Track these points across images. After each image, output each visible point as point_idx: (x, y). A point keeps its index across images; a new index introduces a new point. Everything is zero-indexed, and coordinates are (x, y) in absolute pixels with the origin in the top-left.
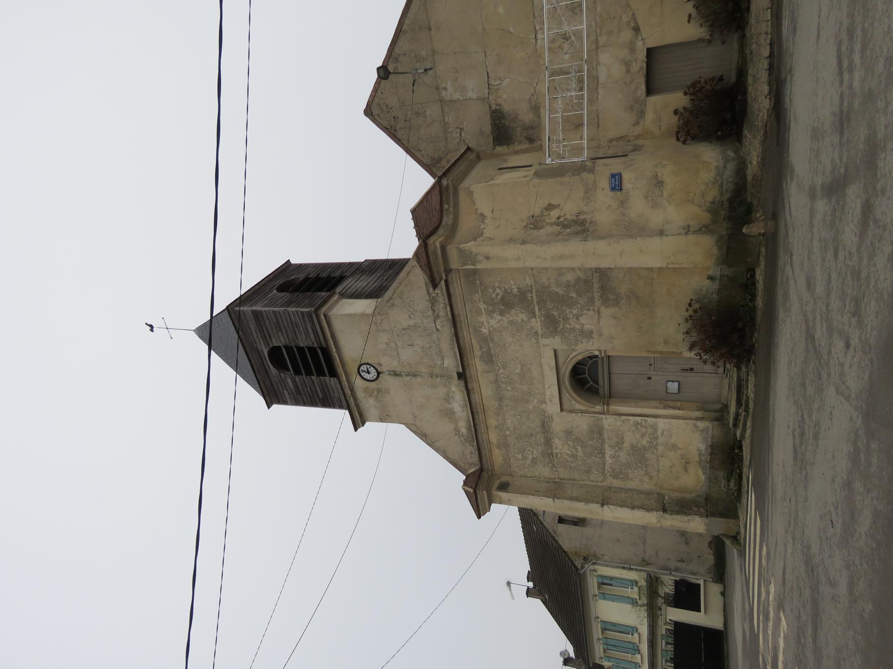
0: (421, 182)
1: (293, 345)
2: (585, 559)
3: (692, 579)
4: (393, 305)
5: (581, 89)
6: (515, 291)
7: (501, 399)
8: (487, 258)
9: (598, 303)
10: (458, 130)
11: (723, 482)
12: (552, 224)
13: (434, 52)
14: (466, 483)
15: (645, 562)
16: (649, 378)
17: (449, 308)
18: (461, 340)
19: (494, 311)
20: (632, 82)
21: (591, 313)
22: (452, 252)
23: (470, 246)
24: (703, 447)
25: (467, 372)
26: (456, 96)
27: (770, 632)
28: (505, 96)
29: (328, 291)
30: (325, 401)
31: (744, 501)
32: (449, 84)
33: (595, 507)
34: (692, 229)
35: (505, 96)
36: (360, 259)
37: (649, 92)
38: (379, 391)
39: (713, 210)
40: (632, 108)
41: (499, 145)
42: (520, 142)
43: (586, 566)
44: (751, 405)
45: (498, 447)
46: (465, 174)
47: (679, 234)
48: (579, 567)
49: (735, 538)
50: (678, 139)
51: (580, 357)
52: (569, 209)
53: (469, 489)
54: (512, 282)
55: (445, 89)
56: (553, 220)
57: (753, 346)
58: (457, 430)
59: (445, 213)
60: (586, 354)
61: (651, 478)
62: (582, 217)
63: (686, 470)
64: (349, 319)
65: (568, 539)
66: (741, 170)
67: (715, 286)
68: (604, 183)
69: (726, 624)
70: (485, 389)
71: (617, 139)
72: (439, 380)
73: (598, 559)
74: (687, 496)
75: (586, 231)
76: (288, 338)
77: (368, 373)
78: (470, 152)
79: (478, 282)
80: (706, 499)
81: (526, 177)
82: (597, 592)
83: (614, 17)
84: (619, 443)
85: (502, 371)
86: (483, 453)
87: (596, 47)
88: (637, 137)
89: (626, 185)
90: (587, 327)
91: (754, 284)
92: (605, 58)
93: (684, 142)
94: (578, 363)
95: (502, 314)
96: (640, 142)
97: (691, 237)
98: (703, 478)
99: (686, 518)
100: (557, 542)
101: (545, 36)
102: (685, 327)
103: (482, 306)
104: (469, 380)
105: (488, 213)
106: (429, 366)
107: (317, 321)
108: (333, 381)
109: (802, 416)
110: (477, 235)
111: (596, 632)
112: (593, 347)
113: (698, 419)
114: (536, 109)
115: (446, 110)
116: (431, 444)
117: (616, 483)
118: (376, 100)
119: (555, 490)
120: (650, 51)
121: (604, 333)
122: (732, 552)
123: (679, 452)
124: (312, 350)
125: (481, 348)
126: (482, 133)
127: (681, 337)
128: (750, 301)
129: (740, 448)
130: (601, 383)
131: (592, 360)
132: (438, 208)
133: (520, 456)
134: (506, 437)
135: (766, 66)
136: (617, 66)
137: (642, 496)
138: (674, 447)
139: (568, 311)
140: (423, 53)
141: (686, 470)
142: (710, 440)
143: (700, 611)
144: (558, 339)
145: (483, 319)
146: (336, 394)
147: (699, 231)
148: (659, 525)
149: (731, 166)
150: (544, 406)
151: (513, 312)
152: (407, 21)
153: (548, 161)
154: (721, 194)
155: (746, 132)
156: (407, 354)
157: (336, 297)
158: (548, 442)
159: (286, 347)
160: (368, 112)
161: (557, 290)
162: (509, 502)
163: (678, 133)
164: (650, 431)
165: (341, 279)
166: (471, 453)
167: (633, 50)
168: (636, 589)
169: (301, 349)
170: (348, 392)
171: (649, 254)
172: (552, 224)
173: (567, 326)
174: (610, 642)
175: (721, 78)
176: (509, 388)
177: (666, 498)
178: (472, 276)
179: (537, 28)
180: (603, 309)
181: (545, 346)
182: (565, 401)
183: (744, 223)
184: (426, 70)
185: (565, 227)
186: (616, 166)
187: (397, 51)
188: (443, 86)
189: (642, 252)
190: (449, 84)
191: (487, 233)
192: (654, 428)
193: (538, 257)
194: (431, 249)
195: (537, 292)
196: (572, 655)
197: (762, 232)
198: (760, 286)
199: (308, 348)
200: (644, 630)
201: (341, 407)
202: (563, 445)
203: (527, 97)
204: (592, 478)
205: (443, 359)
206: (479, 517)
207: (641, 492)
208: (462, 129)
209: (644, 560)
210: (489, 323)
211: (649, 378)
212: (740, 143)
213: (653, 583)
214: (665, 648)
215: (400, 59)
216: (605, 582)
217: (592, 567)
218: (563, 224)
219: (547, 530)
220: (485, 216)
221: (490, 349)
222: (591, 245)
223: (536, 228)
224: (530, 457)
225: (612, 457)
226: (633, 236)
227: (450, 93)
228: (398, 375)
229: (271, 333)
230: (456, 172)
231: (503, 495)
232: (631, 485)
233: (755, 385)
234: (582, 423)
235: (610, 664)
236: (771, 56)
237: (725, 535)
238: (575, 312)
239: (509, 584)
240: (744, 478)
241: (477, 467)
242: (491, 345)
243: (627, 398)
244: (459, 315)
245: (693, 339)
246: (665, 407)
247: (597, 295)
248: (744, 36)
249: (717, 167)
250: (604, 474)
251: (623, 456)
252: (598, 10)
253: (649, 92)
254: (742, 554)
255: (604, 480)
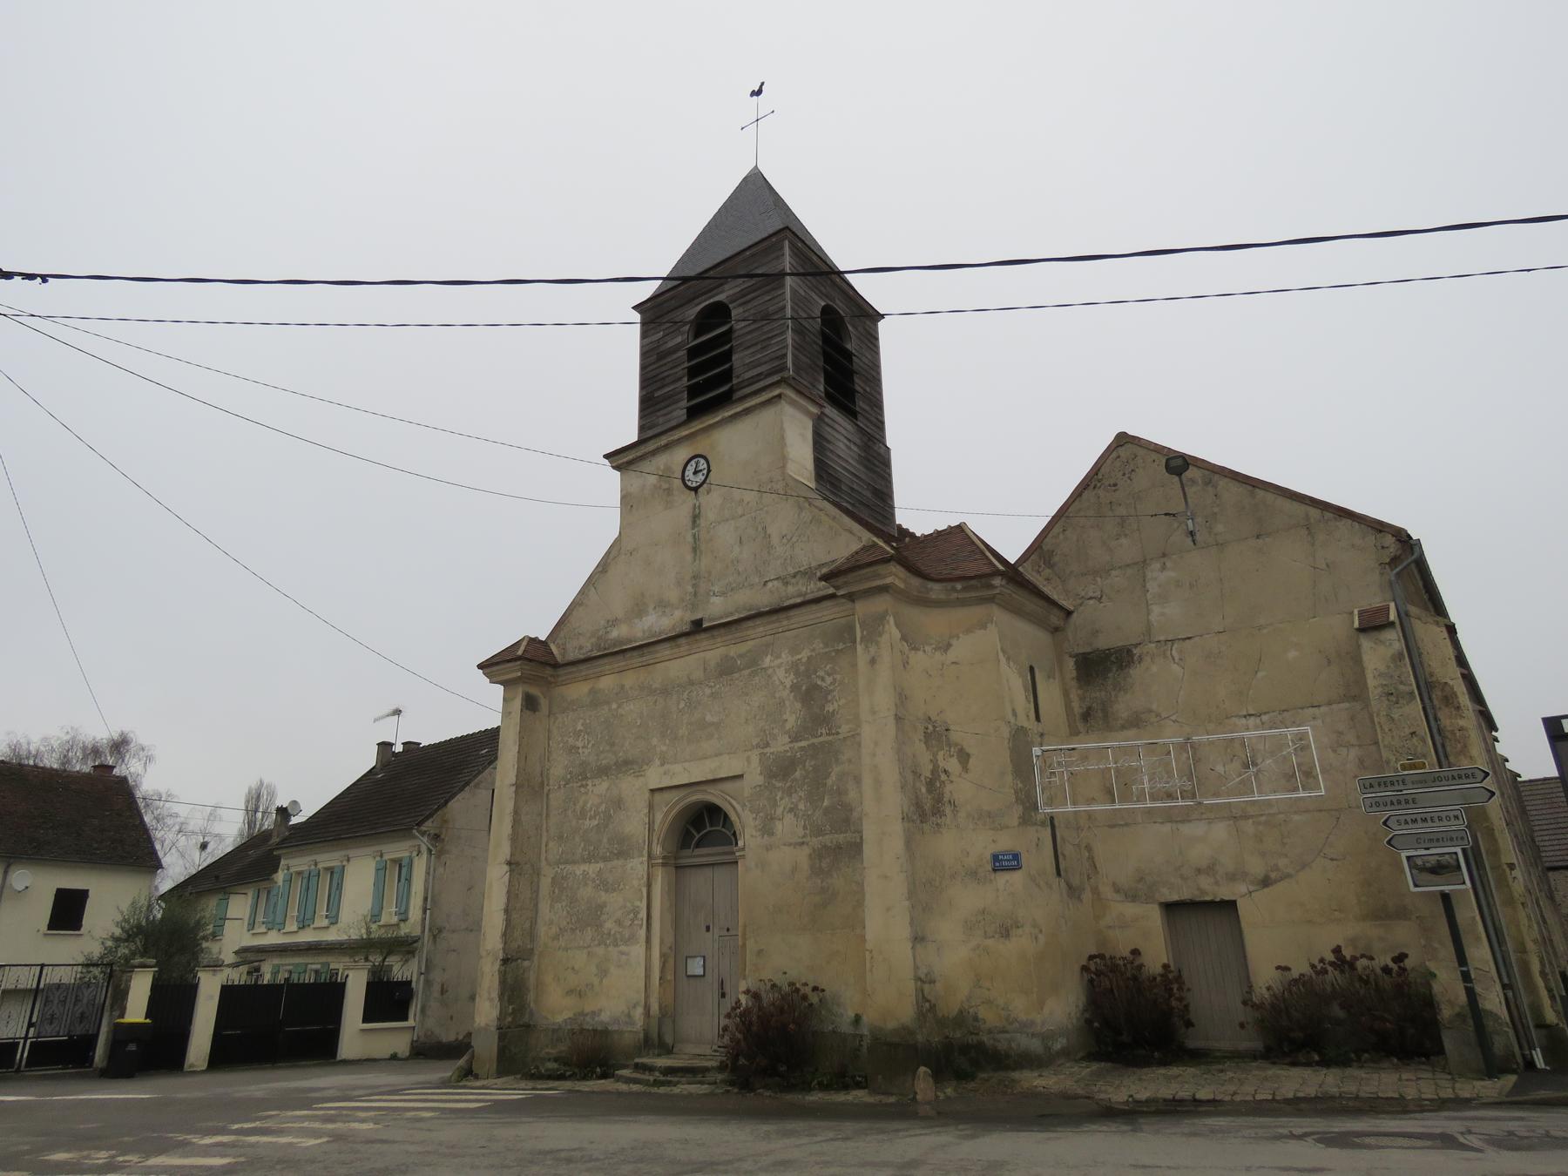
0: (1011, 543)
1: (734, 343)
2: (437, 837)
3: (415, 1009)
4: (801, 509)
5: (1153, 798)
6: (830, 708)
7: (665, 692)
8: (873, 661)
9: (815, 842)
10: (1098, 594)
11: (553, 1052)
12: (934, 762)
13: (1221, 546)
14: (533, 641)
15: (436, 932)
16: (708, 929)
17: (799, 600)
18: (750, 623)
19: (797, 674)
20: (1182, 877)
21: (801, 832)
22: (881, 604)
23: (892, 631)
24: (605, 1017)
25: (703, 636)
26: (1153, 587)
27: (306, 1124)
28: (1154, 669)
29: (827, 394)
30: (649, 403)
31: (523, 1084)
32: (1173, 574)
33: (505, 851)
34: (926, 987)
35: (1154, 669)
36: (891, 439)
37: (1172, 909)
38: (669, 491)
39: (961, 1019)
40: (1141, 879)
41: (1076, 663)
42: (1082, 699)
43: (425, 839)
44: (662, 1090)
45: (592, 691)
46: (1017, 611)
47: (916, 968)
48: (423, 828)
49: (468, 1073)
50: (1091, 958)
51: (733, 817)
52: (961, 788)
53: (522, 648)
54: (843, 701)
55: (1164, 568)
56: (941, 764)
57: (752, 1090)
58: (614, 623)
59: (949, 585)
60: (738, 827)
61: (556, 938)
62: (948, 810)
63: (570, 992)
64: (778, 436)
65: (461, 807)
66: (1029, 1061)
67: (845, 1027)
68: (1005, 843)
69: (345, 1062)
70: (680, 665)
71: (1091, 859)
72: (690, 589)
73: (438, 857)
74: (531, 996)
75: (923, 817)
76: (757, 330)
77: (695, 473)
78: (1062, 615)
79: (841, 646)
80: (528, 1026)
81: (1015, 714)
82: (386, 857)
83: (1284, 844)
84: (605, 885)
85: (708, 691)
86: (582, 667)
87: (1236, 817)
88: (1095, 891)
89: (1003, 879)
90: (779, 826)
91: (846, 1087)
92: (1220, 831)
93: (1085, 969)
94: (726, 816)
95: (795, 688)
96: (1087, 896)
97: (910, 987)
98: (559, 1019)
99: (495, 995)
100: (461, 790)
101: (1252, 733)
102: (780, 980)
103: (804, 655)
104: (691, 639)
105: (952, 655)
106: (710, 573)
107: (774, 381)
108: (680, 413)
109: (597, 1160)
110: (911, 640)
111: (327, 858)
112: (749, 835)
113: (647, 1008)
114: (1136, 722)
115: (1129, 571)
116: (591, 581)
117: (545, 883)
118: (1141, 452)
119: (530, 786)
120: (1232, 905)
121: (771, 853)
122: (447, 1070)
123: (596, 981)
124: (727, 376)
125: (741, 656)
126: (1095, 633)
127: (767, 975)
128: (819, 1084)
129: (604, 1076)
130: (699, 851)
131: (731, 838)
132: (958, 573)
133: (579, 727)
134: (608, 703)
135: (1182, 1094)
136: (1205, 851)
137: (527, 925)
138: (603, 972)
139: (802, 794)
140: (1220, 528)
141: (570, 992)
142: (615, 1028)
143: (365, 1020)
144: (760, 780)
145: (786, 657)
146: (661, 420)
147: (922, 998)
148: (484, 953)
149: (1035, 1046)
150: (657, 762)
151: (798, 705)
152: (1270, 497)
153: (1036, 751)
154: (990, 1031)
155: (1095, 1066)
156: (725, 535)
157: (814, 410)
158: (603, 772)
159: (730, 331)
160: (1123, 440)
161: (833, 777)
162: (506, 713)
163: (1101, 956)
164: (627, 934)
165: (851, 413)
166: (581, 648)
167: (1232, 877)
168: (395, 920)
169: (727, 356)
170: (663, 441)
171: (885, 919)
172: (934, 762)
173: (779, 794)
174: (314, 880)
175: (1189, 1024)
176: (682, 705)
177: (526, 963)
178: (846, 634)
179: (1265, 718)
180: (806, 850)
181: (748, 759)
182: (667, 796)
183: (956, 1065)
184: (1192, 534)
185: (930, 784)
186: (1038, 859)
187: (1222, 482)
188: (1168, 564)
189: (888, 909)
190: (1173, 574)
191: (919, 659)
192: (631, 940)
193: (876, 744)
194: (881, 569)
195: (830, 743)
196: (294, 821)
197: (918, 1097)
198: (841, 1097)
199: (731, 369)
200: (332, 936)
201: (642, 429)
202: (600, 796)
203: (1154, 707)
204: (551, 844)
205: (723, 594)
206: (480, 666)
207: (534, 922)
208: (1099, 599)
209: (440, 931)
210: (780, 668)
211: (708, 929)
212: (1083, 1059)
213: (405, 946)
214: (308, 970)
215: (1210, 489)
216: (403, 868)
217: (424, 849)
218: (934, 783)
219: (480, 773)
220: (946, 651)
221: (740, 670)
222: (897, 828)
223: (928, 737)
224: (580, 744)
225: (585, 874)
226: (911, 894)
227: (1158, 577)
228: (694, 522)
229: (749, 306)
230: (1021, 597)
231: (518, 703)
232: (544, 907)
233: (691, 1094)
234: (634, 824)
235: (280, 883)
236: (1196, 1102)
237: (473, 1056)
238: (801, 806)
239: (397, 712)
240: (556, 1084)
241: (559, 659)
242: (746, 672)
243: (677, 894)
244: (788, 618)
245: (764, 995)
246: (663, 956)
247: (827, 839)
248: (1255, 1058)
249: (1033, 1023)
250: (558, 863)
251: (586, 892)
252: (1296, 818)
253: (1170, 908)
254: (444, 1084)
255: (549, 864)
